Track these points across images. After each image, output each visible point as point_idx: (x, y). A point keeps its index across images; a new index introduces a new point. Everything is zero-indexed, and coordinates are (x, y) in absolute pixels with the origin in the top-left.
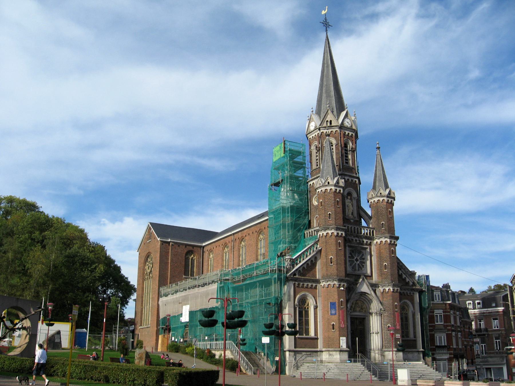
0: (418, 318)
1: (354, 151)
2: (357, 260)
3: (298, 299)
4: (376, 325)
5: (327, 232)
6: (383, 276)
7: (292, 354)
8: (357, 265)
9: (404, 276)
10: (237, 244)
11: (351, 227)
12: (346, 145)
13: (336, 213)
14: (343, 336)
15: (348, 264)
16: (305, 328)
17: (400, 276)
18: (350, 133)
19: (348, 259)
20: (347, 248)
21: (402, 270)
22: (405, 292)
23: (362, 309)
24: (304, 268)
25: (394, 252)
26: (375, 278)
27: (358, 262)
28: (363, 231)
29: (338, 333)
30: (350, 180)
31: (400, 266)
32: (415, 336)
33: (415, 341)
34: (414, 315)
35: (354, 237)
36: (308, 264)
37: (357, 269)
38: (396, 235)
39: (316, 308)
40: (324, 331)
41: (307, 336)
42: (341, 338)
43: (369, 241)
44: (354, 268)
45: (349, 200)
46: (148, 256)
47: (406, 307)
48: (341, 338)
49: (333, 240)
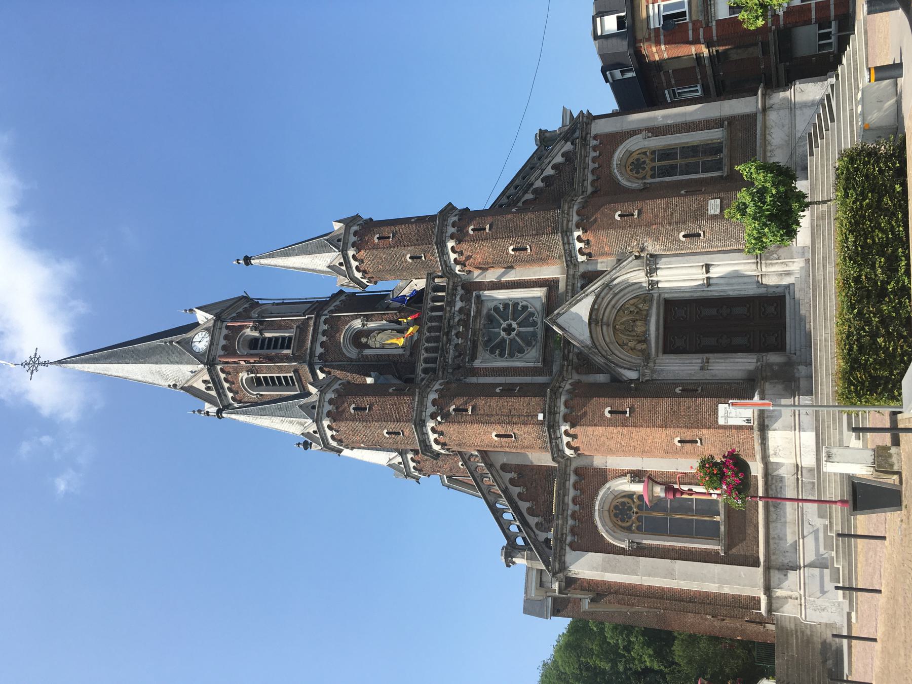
0: (664, 117)
2: (509, 330)
3: (615, 538)
4: (684, 271)
6: (544, 255)
8: (522, 329)
9: (549, 171)
11: (427, 350)
12: (254, 343)
13: (385, 418)
14: (715, 412)
16: (698, 512)
18: (225, 332)
20: (477, 364)
21: (532, 178)
22: (592, 166)
24: (531, 512)
26: (553, 271)
27: (515, 325)
29: (705, 431)
30: (324, 339)
32: (717, 123)
33: (730, 123)
35: (449, 341)
43: (460, 291)
44: (529, 340)
47: (635, 156)
48: (721, 422)
49: (452, 431)
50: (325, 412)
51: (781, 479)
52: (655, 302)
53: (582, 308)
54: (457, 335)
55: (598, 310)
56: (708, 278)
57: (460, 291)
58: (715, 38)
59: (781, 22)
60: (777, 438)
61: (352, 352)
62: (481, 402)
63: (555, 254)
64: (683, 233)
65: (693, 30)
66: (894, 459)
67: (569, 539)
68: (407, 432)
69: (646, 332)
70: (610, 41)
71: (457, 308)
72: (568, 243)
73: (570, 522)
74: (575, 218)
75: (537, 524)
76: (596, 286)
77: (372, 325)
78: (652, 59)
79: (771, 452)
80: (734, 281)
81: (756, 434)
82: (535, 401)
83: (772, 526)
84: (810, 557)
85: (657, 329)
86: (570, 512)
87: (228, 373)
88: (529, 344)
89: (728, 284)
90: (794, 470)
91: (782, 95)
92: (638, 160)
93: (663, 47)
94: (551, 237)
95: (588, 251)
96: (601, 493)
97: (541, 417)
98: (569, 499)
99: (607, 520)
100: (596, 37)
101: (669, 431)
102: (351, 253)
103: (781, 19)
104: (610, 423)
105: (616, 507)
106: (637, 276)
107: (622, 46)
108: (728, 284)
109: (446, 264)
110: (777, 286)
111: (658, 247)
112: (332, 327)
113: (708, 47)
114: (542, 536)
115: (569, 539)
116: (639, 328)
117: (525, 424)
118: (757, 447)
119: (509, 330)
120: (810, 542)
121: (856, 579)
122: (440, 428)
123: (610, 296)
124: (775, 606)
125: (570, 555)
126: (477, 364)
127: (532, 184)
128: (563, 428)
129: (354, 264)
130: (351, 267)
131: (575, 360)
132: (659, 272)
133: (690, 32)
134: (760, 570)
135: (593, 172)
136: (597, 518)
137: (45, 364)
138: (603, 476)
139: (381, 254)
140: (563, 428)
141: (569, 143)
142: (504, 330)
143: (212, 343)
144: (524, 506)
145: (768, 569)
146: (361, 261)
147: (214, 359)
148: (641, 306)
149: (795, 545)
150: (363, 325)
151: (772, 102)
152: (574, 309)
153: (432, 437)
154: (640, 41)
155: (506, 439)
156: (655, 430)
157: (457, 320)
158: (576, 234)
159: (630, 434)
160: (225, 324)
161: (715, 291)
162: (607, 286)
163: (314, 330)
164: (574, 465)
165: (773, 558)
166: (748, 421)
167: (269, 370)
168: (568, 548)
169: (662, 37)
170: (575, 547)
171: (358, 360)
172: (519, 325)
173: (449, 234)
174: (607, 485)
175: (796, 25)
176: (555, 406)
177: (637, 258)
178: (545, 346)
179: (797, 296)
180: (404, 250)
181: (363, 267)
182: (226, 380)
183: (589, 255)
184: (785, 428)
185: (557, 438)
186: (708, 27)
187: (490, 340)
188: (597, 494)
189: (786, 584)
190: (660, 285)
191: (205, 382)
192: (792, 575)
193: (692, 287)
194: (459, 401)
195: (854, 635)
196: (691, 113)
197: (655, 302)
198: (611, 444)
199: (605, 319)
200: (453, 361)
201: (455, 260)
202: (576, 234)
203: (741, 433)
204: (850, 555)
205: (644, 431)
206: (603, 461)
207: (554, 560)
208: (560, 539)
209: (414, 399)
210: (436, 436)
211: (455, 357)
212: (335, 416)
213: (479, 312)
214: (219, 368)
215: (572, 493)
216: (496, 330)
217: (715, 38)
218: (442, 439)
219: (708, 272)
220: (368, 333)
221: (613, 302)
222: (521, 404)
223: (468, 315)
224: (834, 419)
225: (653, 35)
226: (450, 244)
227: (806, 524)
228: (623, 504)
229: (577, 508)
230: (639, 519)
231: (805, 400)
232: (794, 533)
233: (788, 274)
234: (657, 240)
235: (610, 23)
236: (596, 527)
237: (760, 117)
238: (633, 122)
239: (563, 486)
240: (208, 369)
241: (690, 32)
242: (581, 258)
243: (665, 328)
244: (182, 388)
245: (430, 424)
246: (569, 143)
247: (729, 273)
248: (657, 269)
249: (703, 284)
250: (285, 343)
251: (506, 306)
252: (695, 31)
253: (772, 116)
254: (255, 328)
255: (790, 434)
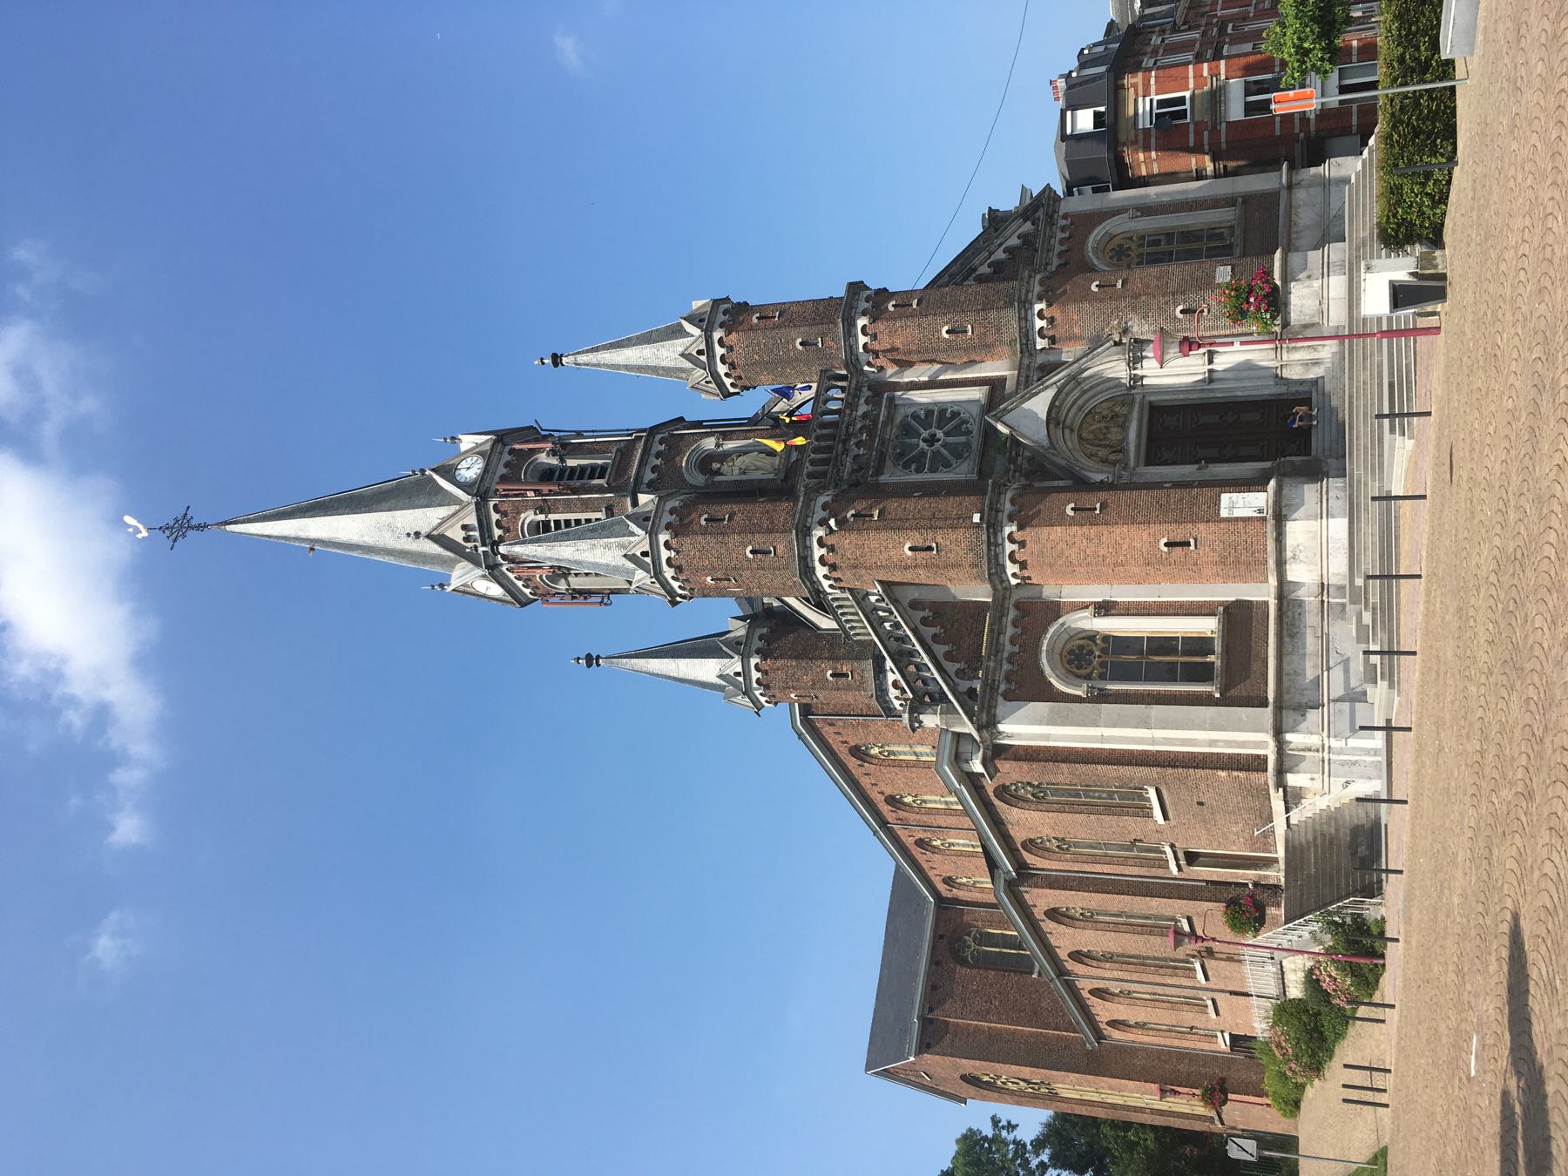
1: (564, 448)
2: (932, 440)
3: (1068, 684)
5: (817, 564)
6: (990, 340)
7: (1289, 717)
8: (950, 439)
9: (1000, 255)
10: (912, 817)
12: (547, 475)
13: (750, 529)
14: (1217, 503)
15: (943, 476)
16: (1186, 653)
17: (1001, 271)
18: (506, 457)
19: (926, 476)
20: (883, 478)
21: (976, 262)
22: (1058, 248)
23: (1115, 416)
24: (949, 656)
25: (903, 299)
26: (998, 367)
27: (940, 434)
28: (833, 406)
29: (1202, 526)
31: (959, 272)
32: (1230, 201)
33: (1247, 199)
34: (1146, 210)
35: (846, 451)
36: (935, 637)
37: (963, 439)
38: (840, 292)
39: (1105, 609)
40: (1194, 572)
41: (1218, 646)
42: (1224, 513)
43: (866, 393)
44: (958, 452)
45: (725, 468)
46: (972, 1080)
47: (1117, 241)
48: (1224, 513)
49: (848, 543)
50: (664, 523)
51: (1301, 603)
52: (1137, 406)
53: (1039, 405)
54: (858, 445)
55: (1059, 407)
56: (1210, 371)
57: (866, 393)
58: (1224, 146)
59: (1312, 128)
60: (1298, 531)
61: (699, 479)
62: (893, 505)
63: (1006, 338)
64: (1181, 307)
65: (1196, 133)
66: (1439, 261)
67: (1003, 687)
68: (781, 549)
69: (1125, 439)
70: (1082, 143)
71: (860, 413)
72: (1025, 320)
73: (1006, 666)
74: (1037, 289)
75: (957, 673)
76: (1059, 377)
77: (730, 445)
78: (1137, 174)
79: (1289, 554)
80: (1245, 374)
81: (1271, 523)
82: (968, 501)
83: (1285, 660)
84: (1338, 690)
85: (1139, 436)
86: (1006, 655)
87: (504, 514)
88: (959, 456)
89: (1236, 379)
90: (1317, 590)
91: (1313, 170)
92: (1121, 246)
93: (1153, 154)
94: (1002, 313)
95: (1051, 333)
96: (1051, 630)
97: (976, 518)
98: (1005, 640)
99: (1059, 665)
100: (1064, 137)
101: (1154, 528)
102: (717, 335)
103: (1313, 123)
104: (1072, 522)
105: (1071, 652)
106: (1114, 368)
107: (1102, 152)
108: (1236, 379)
109: (851, 348)
110: (1302, 382)
111: (1146, 327)
112: (670, 448)
113: (1214, 160)
114: (964, 685)
115: (1003, 687)
116: (1115, 435)
117: (954, 528)
118: (1271, 546)
119: (932, 440)
120: (1337, 674)
121: (1397, 562)
122: (830, 541)
123: (1076, 393)
124: (1287, 764)
125: (1002, 706)
126: (883, 478)
127: (975, 269)
128: (1007, 530)
129: (719, 351)
130: (714, 356)
131: (1025, 465)
132: (1145, 363)
133: (1192, 136)
134: (1268, 712)
135: (1060, 255)
136: (1044, 660)
137: (201, 527)
138: (1055, 610)
139: (760, 338)
140: (1007, 530)
141: (1029, 224)
142: (925, 440)
143: (486, 470)
144: (940, 650)
145: (1279, 708)
146: (730, 349)
147: (486, 492)
148: (1117, 409)
149: (1317, 682)
150: (718, 445)
151: (1300, 177)
152: (1026, 405)
153: (818, 552)
154: (1124, 144)
155: (923, 554)
156: (1134, 528)
157: (859, 426)
158: (1038, 307)
159: (1099, 536)
160: (507, 448)
161: (1220, 392)
162: (1074, 379)
163: (644, 450)
164: (1015, 597)
165: (1286, 697)
166: (1260, 511)
167: (568, 507)
168: (1000, 699)
169: (1153, 140)
170: (1008, 697)
171: (706, 486)
172: (947, 434)
173: (860, 309)
174: (1061, 621)
175: (1331, 136)
176: (998, 501)
177: (1116, 344)
178: (983, 455)
179: (1327, 388)
180: (793, 333)
181: (733, 357)
182: (498, 524)
183: (1053, 340)
184: (1308, 518)
185: (997, 545)
186: (1215, 132)
187: (901, 455)
188: (1045, 631)
189: (1303, 726)
190: (1145, 382)
191: (464, 527)
192: (1313, 715)
193: (1187, 385)
194: (861, 505)
195: (1395, 797)
196: (1195, 190)
197: (1137, 406)
198: (1072, 554)
199: (1068, 421)
200: (850, 474)
201: (865, 345)
202: (1038, 307)
203: (1250, 527)
204: (1390, 619)
205: (1119, 531)
206: (1057, 591)
207: (981, 710)
208: (990, 687)
209: (795, 505)
210: (823, 551)
211: (854, 471)
212: (677, 530)
213: (890, 418)
214: (491, 504)
215: (1010, 631)
216: (914, 441)
217: (1224, 146)
218: (831, 558)
219: (1211, 362)
220: (724, 457)
221: (1080, 402)
222: (949, 505)
223: (875, 422)
224: (1373, 470)
225: (1141, 137)
226: (861, 322)
227: (1332, 653)
228: (1081, 647)
229: (1016, 649)
230: (1102, 665)
231: (1335, 485)
232: (1316, 666)
233: (1316, 363)
234: (1145, 317)
235: (1084, 120)
236: (1042, 672)
237: (1284, 194)
238: (1117, 200)
239: (996, 633)
240: (477, 504)
241: (1192, 136)
242: (1041, 343)
243: (1150, 439)
244: (429, 536)
245: (819, 532)
246: (1029, 224)
247: (1239, 364)
248: (1143, 358)
249: (1203, 381)
250: (601, 472)
251: (929, 413)
252: (1198, 134)
253: (1300, 195)
254: (553, 453)
255: (1314, 525)
